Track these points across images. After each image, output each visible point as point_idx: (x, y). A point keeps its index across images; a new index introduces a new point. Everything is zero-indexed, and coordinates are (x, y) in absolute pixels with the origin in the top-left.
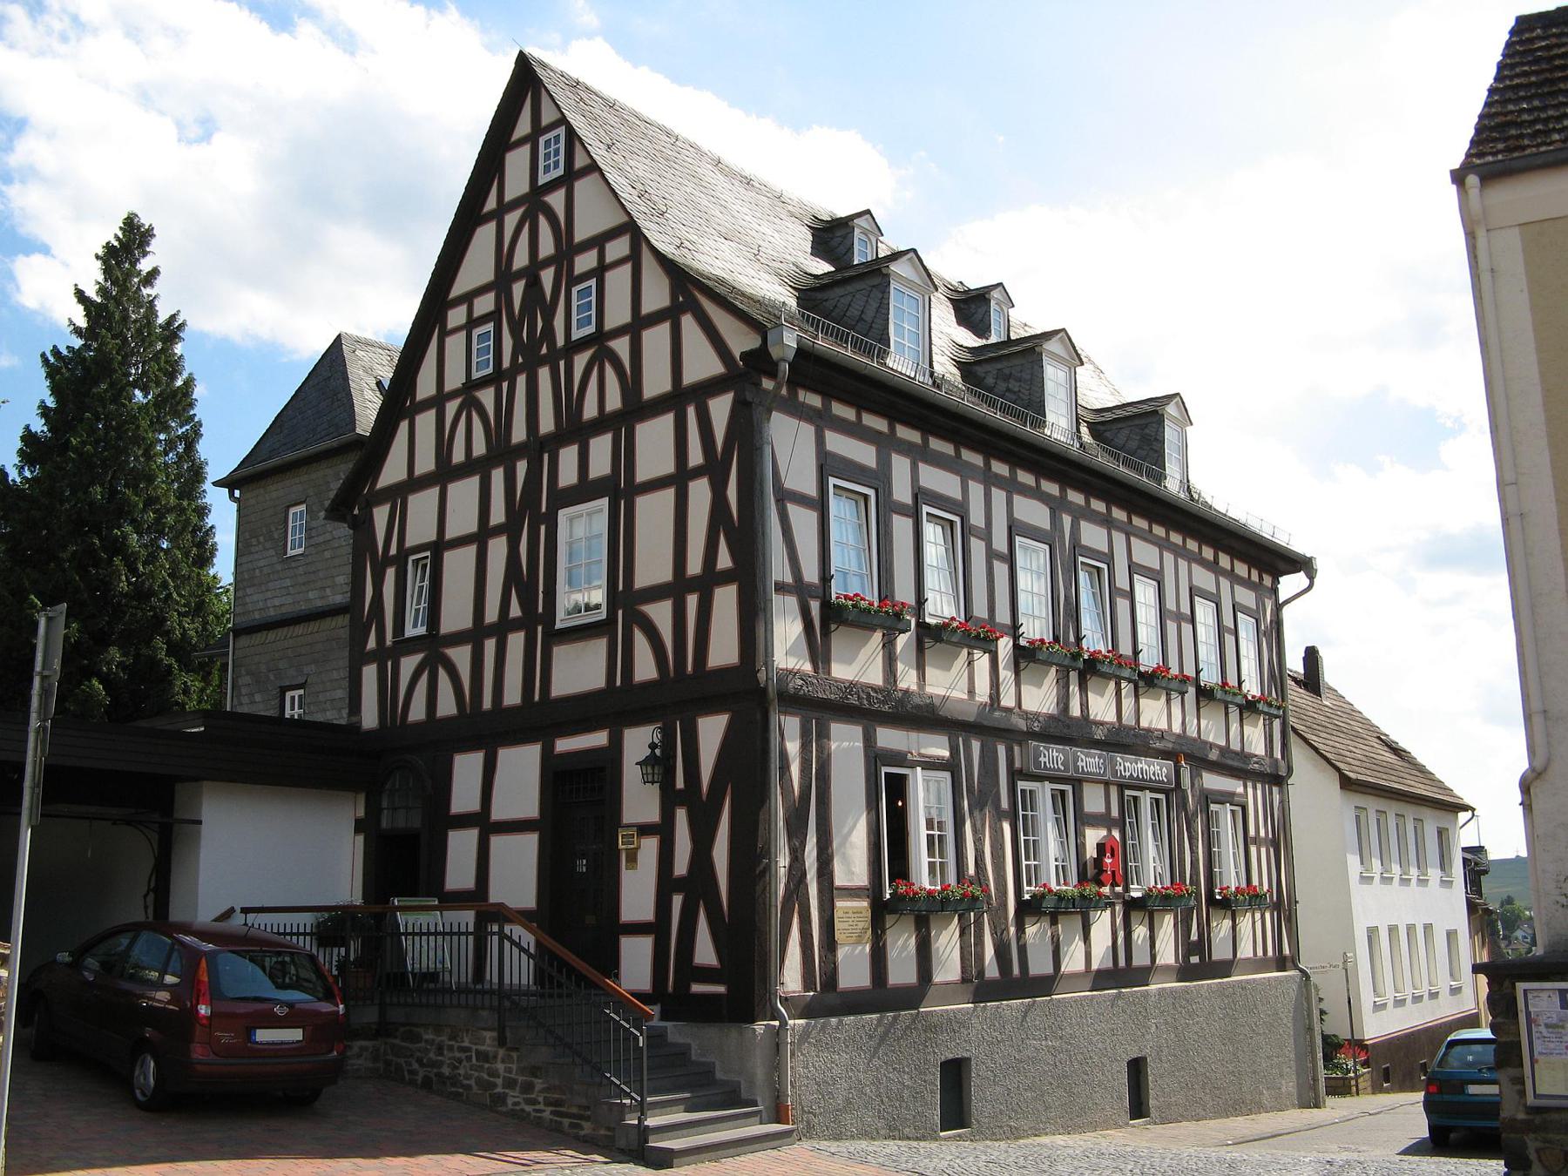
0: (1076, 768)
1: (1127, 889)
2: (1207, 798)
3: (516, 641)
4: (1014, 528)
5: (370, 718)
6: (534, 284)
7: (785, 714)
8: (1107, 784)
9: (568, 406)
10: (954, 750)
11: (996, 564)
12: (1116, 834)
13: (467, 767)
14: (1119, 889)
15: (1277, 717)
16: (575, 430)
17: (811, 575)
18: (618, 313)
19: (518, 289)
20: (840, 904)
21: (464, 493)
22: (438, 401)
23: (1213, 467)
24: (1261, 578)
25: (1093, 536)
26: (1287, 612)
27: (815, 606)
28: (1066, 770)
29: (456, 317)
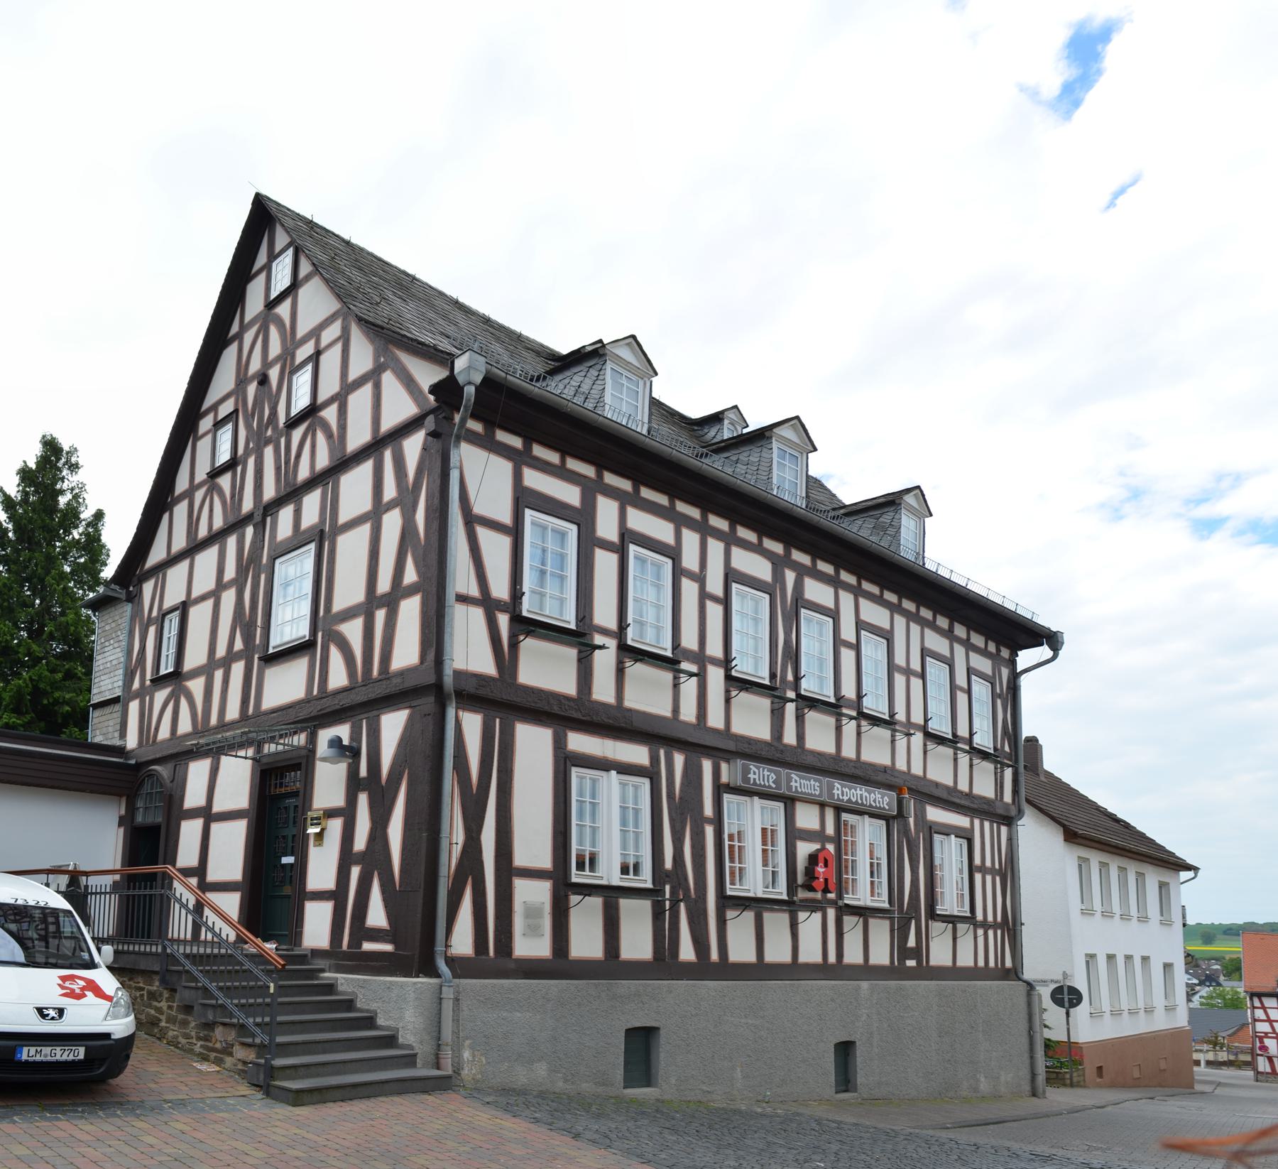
0: (789, 788)
1: (840, 897)
2: (932, 830)
3: (238, 669)
4: (731, 576)
5: (132, 742)
6: (263, 380)
7: (464, 709)
8: (822, 805)
9: (286, 468)
10: (654, 759)
11: (709, 604)
12: (831, 848)
13: (198, 771)
14: (832, 896)
15: (1009, 766)
16: (292, 494)
17: (500, 590)
18: (329, 386)
19: (252, 389)
20: (520, 885)
21: (207, 559)
22: (189, 494)
23: (951, 549)
24: (998, 650)
25: (817, 591)
26: (1024, 681)
27: (503, 620)
28: (778, 787)
29: (206, 424)
